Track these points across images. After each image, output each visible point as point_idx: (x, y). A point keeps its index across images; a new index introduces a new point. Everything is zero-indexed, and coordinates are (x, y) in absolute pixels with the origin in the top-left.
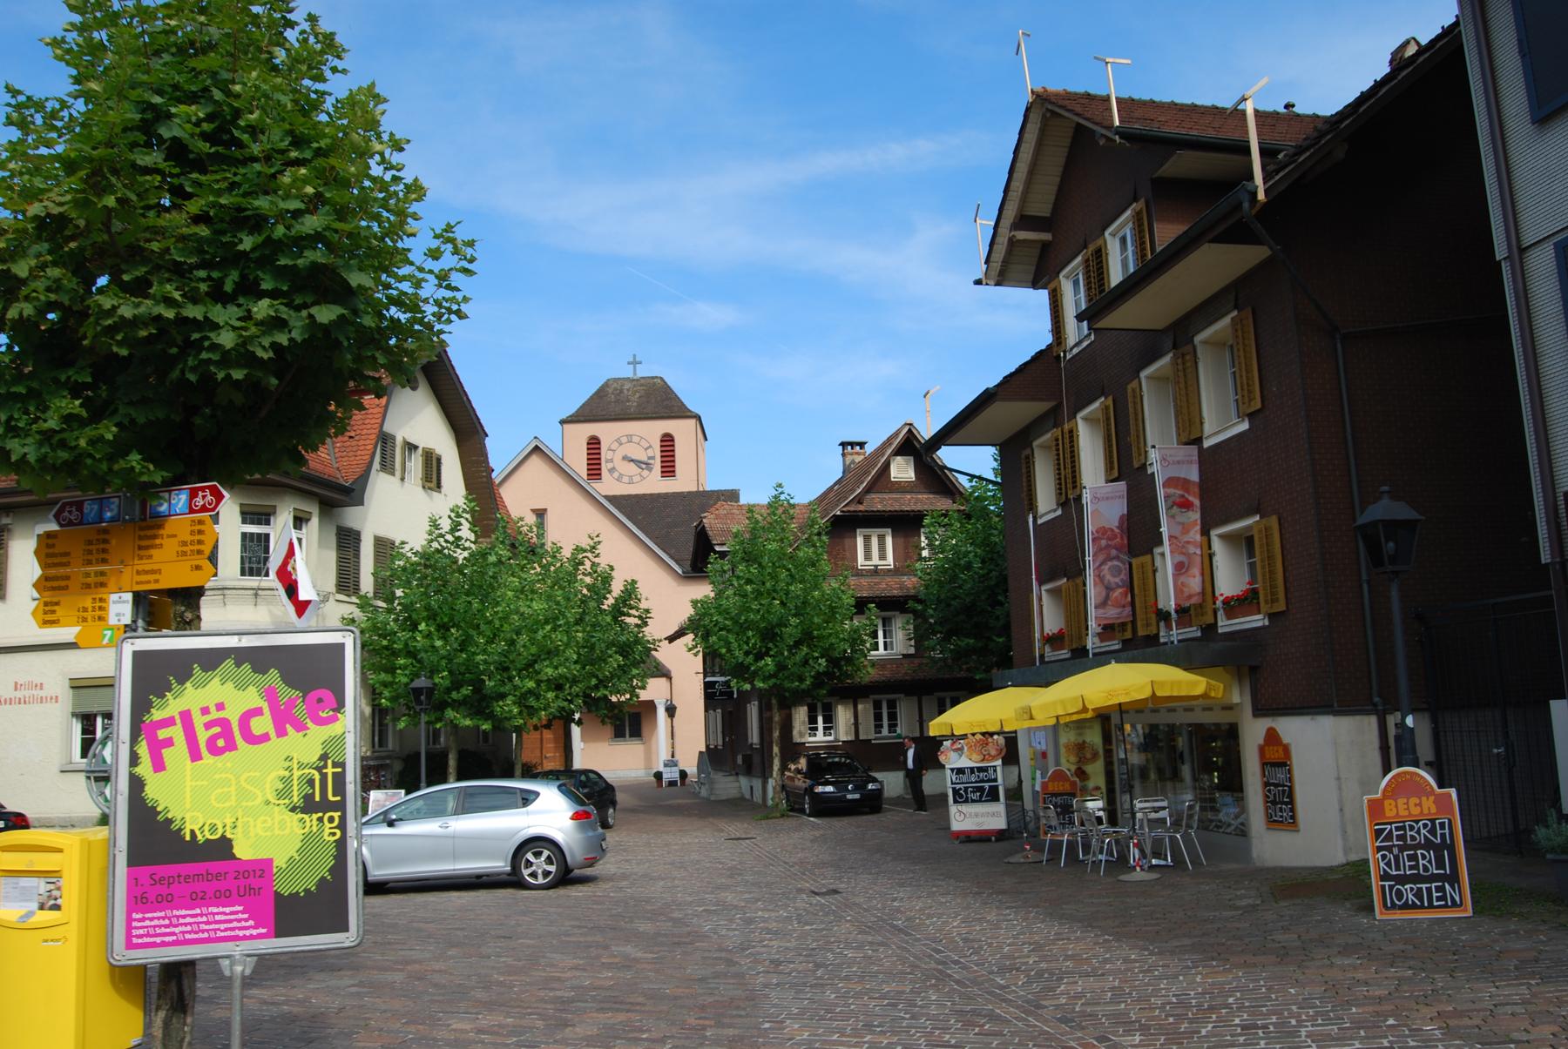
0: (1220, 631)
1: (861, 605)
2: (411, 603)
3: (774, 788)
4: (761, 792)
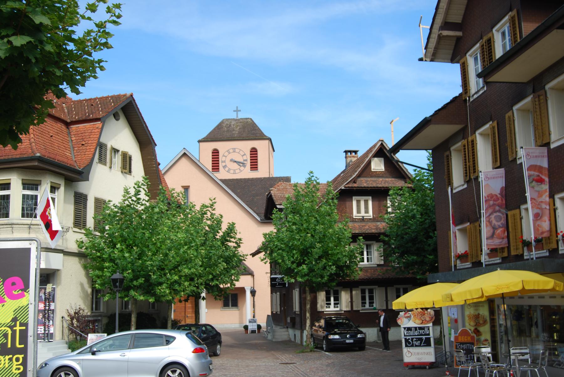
0: (560, 252)
1: (355, 238)
2: (113, 233)
3: (307, 336)
4: (300, 337)
